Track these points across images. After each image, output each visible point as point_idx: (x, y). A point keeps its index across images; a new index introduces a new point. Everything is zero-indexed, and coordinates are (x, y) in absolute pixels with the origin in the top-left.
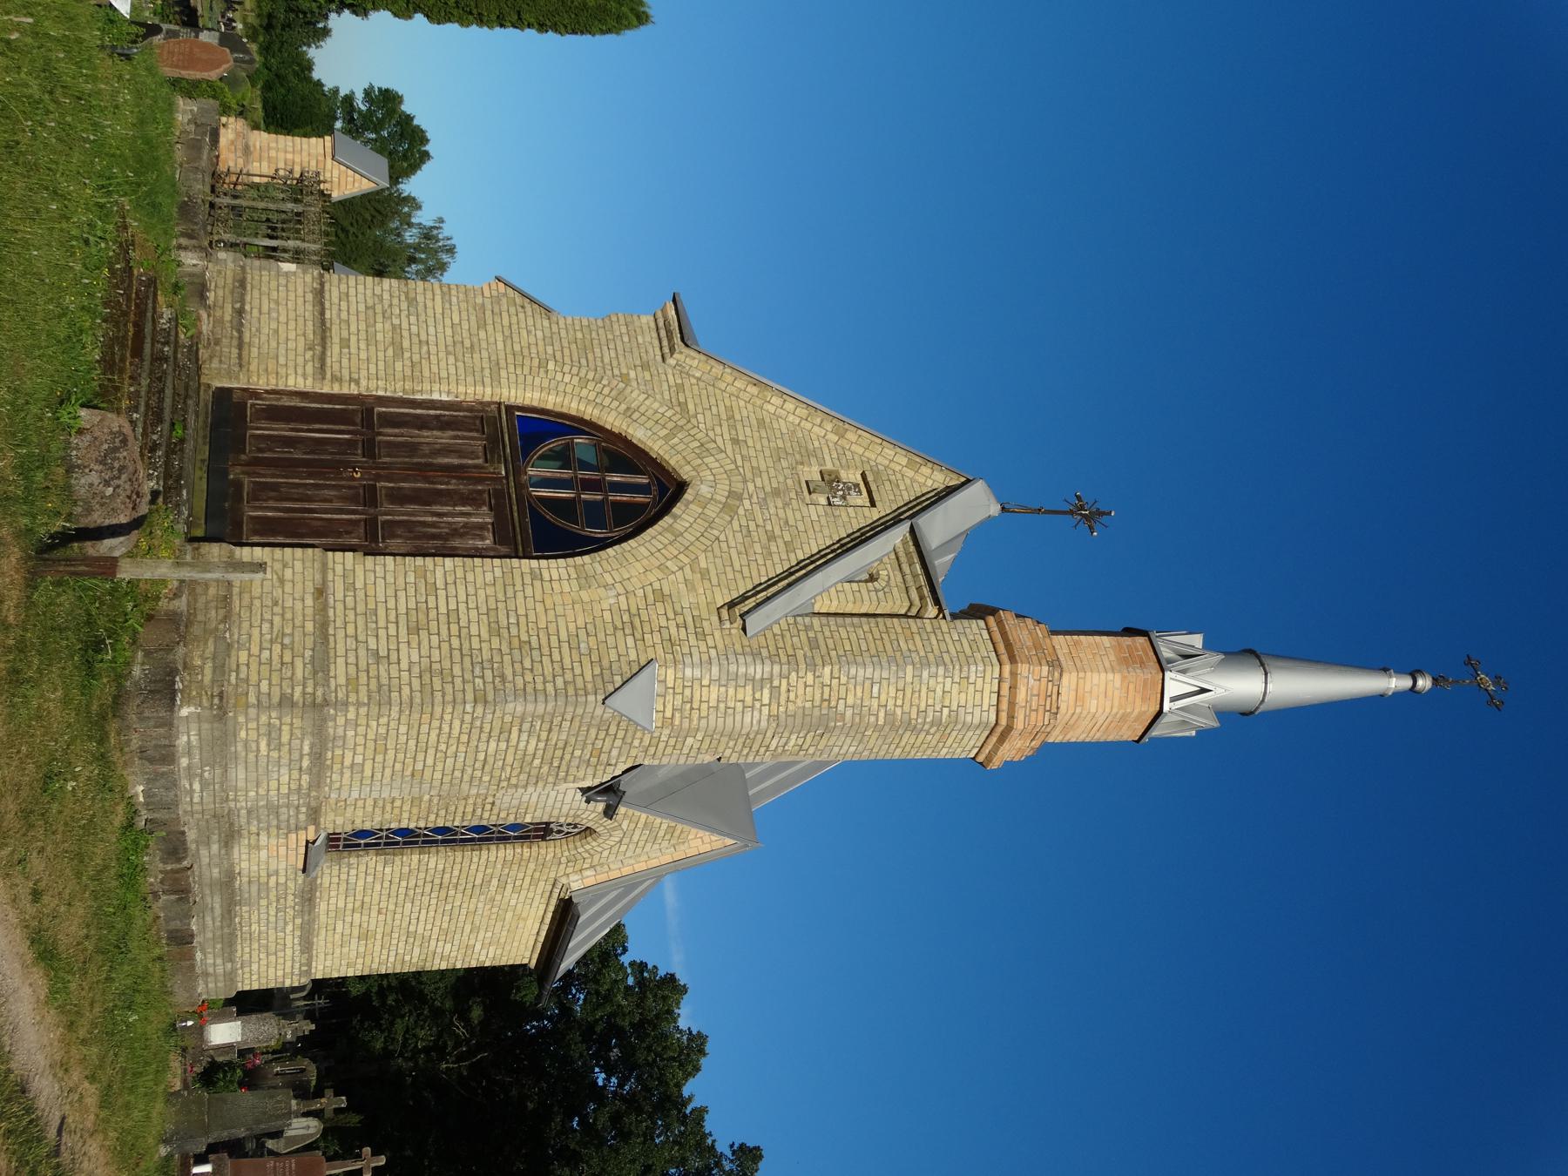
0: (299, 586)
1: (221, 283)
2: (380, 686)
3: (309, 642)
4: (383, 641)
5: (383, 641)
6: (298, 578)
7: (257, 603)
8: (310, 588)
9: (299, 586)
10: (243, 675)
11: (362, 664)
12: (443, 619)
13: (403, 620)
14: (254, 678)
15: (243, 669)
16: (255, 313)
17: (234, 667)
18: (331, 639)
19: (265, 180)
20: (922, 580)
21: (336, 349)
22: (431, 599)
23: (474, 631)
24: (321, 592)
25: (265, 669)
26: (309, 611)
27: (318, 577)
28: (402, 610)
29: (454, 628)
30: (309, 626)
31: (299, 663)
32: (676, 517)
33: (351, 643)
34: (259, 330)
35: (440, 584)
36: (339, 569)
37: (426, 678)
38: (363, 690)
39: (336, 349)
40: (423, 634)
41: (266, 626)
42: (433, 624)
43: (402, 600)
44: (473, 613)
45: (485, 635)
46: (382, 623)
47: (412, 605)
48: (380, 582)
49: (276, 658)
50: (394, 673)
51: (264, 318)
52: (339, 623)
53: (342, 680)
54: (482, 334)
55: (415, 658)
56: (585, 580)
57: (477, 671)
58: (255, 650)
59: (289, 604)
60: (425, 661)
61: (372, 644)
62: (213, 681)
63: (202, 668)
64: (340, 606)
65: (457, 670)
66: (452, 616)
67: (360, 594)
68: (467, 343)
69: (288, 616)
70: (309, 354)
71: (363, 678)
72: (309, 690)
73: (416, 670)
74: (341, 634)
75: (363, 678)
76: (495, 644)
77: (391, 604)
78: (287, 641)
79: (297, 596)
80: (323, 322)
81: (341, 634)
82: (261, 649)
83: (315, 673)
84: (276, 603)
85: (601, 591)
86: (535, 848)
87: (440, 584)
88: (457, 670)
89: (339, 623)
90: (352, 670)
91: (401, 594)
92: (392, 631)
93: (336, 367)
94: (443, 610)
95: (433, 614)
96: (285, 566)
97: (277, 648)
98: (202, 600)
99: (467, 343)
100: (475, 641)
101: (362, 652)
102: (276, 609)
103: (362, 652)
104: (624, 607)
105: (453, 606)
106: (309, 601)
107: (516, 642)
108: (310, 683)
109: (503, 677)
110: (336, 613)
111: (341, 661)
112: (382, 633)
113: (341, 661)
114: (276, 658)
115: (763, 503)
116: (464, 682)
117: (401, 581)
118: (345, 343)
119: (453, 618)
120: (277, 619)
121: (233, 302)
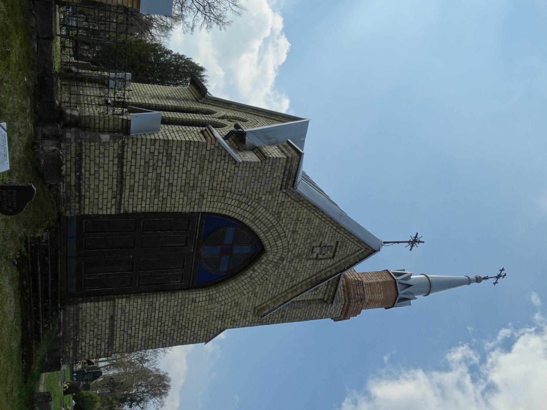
0: (104, 317)
1: (69, 158)
2: (131, 346)
3: (107, 336)
4: (133, 331)
5: (133, 331)
6: (104, 313)
7: (88, 325)
8: (108, 316)
9: (104, 317)
10: (83, 350)
11: (125, 339)
12: (156, 321)
13: (141, 322)
14: (87, 351)
15: (84, 348)
16: (87, 175)
17: (80, 348)
18: (115, 332)
19: (100, 360)
20: (332, 294)
21: (127, 192)
22: (153, 314)
23: (166, 324)
24: (112, 318)
25: (91, 348)
26: (108, 326)
27: (111, 312)
28: (142, 319)
29: (160, 323)
30: (107, 331)
31: (103, 344)
32: (254, 271)
33: (122, 333)
34: (89, 187)
35: (157, 308)
36: (120, 306)
37: (147, 341)
38: (125, 348)
39: (127, 192)
40: (148, 327)
41: (91, 333)
42: (152, 323)
43: (142, 316)
44: (167, 317)
45: (170, 325)
46: (134, 324)
47: (146, 316)
48: (135, 309)
49: (95, 343)
50: (136, 341)
51: (92, 178)
52: (118, 326)
53: (117, 346)
54: (200, 176)
55: (144, 335)
56: (211, 300)
57: (165, 337)
58: (88, 341)
59: (100, 323)
60: (147, 336)
61: (129, 332)
62: (73, 356)
63: (69, 352)
64: (119, 320)
65: (158, 338)
66: (160, 319)
67: (127, 315)
68: (191, 184)
69: (100, 328)
70: (114, 200)
71: (125, 344)
72: (106, 352)
73: (144, 339)
74: (118, 330)
75: (125, 343)
76: (173, 328)
77: (138, 317)
78: (99, 337)
79: (103, 320)
80: (122, 172)
81: (118, 330)
82: (90, 340)
83: (109, 346)
84: (95, 324)
85: (216, 305)
86: (177, 294)
87: (157, 308)
88: (158, 338)
89: (118, 326)
90: (121, 342)
91: (142, 313)
92: (137, 327)
93: (126, 205)
94: (157, 317)
95: (152, 320)
96: (99, 309)
97: (95, 340)
98: (68, 328)
99: (191, 184)
100: (166, 327)
101: (126, 336)
102: (95, 326)
103: (126, 336)
104: (222, 310)
105: (160, 315)
106: (108, 322)
107: (180, 326)
108: (107, 350)
109: (173, 338)
110: (118, 323)
111: (118, 339)
112: (133, 328)
113: (118, 339)
114: (95, 343)
115: (291, 262)
116: (159, 342)
117: (143, 308)
118: (132, 189)
119: (160, 320)
120: (96, 330)
121: (76, 172)
